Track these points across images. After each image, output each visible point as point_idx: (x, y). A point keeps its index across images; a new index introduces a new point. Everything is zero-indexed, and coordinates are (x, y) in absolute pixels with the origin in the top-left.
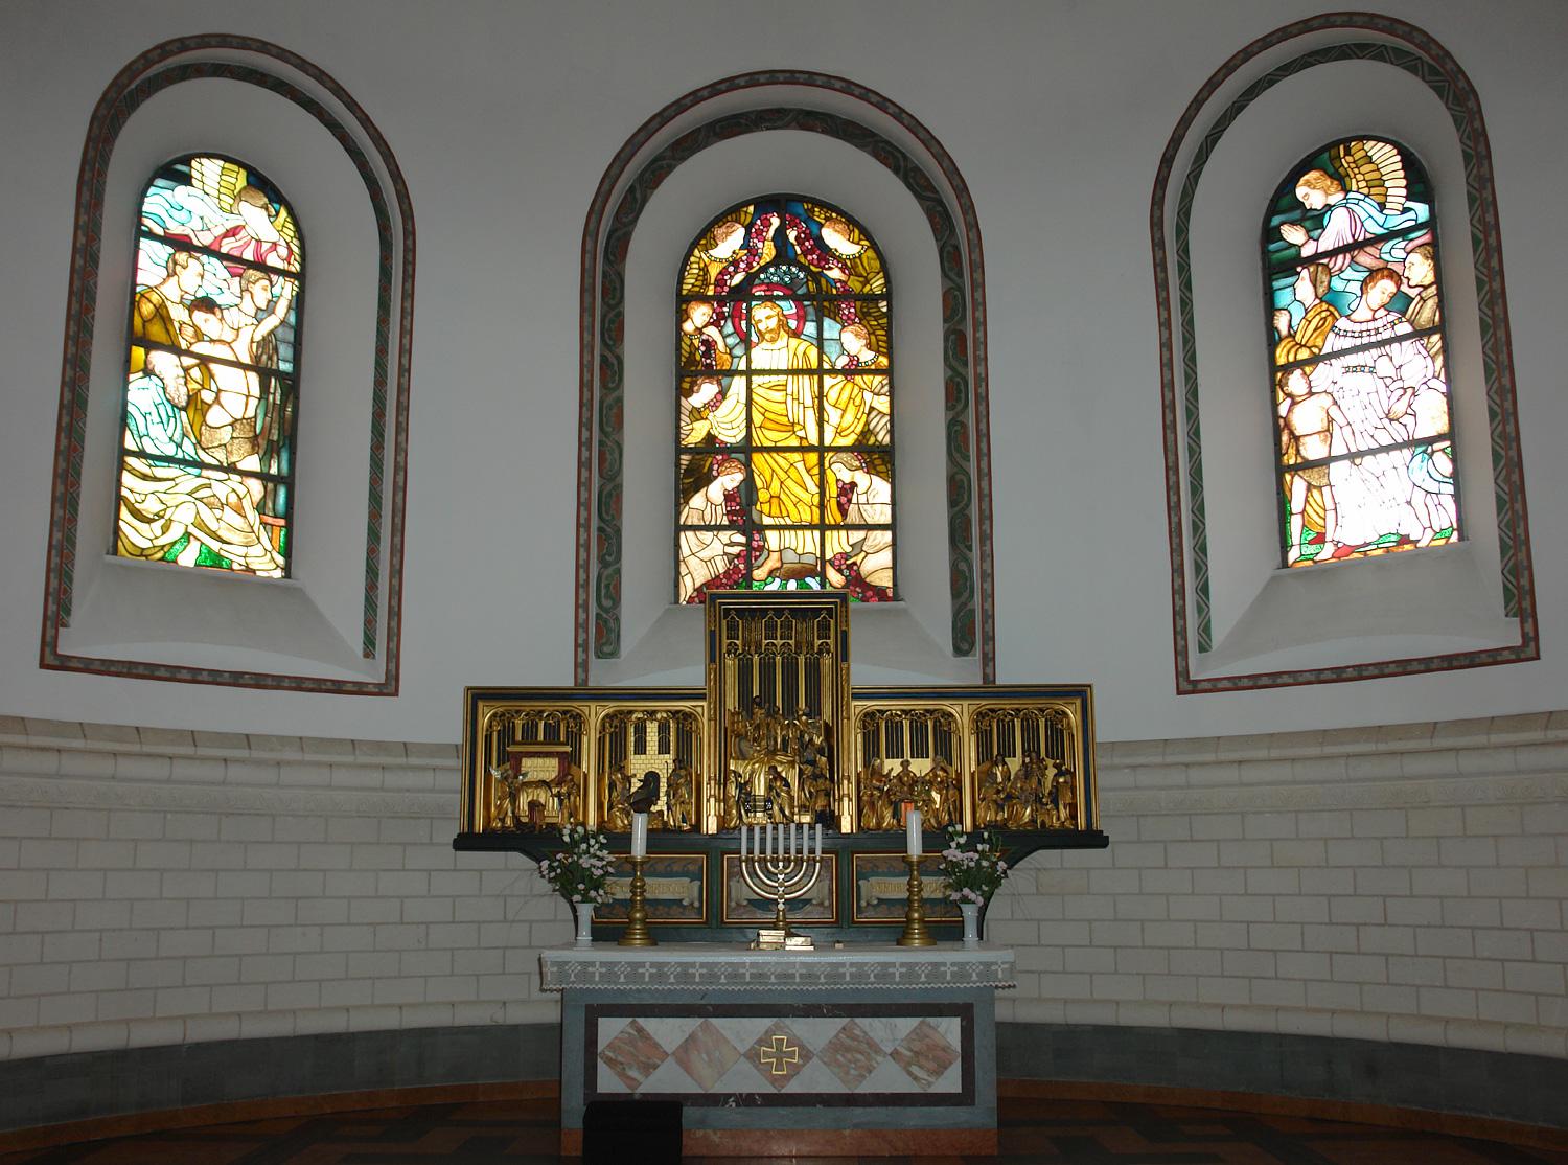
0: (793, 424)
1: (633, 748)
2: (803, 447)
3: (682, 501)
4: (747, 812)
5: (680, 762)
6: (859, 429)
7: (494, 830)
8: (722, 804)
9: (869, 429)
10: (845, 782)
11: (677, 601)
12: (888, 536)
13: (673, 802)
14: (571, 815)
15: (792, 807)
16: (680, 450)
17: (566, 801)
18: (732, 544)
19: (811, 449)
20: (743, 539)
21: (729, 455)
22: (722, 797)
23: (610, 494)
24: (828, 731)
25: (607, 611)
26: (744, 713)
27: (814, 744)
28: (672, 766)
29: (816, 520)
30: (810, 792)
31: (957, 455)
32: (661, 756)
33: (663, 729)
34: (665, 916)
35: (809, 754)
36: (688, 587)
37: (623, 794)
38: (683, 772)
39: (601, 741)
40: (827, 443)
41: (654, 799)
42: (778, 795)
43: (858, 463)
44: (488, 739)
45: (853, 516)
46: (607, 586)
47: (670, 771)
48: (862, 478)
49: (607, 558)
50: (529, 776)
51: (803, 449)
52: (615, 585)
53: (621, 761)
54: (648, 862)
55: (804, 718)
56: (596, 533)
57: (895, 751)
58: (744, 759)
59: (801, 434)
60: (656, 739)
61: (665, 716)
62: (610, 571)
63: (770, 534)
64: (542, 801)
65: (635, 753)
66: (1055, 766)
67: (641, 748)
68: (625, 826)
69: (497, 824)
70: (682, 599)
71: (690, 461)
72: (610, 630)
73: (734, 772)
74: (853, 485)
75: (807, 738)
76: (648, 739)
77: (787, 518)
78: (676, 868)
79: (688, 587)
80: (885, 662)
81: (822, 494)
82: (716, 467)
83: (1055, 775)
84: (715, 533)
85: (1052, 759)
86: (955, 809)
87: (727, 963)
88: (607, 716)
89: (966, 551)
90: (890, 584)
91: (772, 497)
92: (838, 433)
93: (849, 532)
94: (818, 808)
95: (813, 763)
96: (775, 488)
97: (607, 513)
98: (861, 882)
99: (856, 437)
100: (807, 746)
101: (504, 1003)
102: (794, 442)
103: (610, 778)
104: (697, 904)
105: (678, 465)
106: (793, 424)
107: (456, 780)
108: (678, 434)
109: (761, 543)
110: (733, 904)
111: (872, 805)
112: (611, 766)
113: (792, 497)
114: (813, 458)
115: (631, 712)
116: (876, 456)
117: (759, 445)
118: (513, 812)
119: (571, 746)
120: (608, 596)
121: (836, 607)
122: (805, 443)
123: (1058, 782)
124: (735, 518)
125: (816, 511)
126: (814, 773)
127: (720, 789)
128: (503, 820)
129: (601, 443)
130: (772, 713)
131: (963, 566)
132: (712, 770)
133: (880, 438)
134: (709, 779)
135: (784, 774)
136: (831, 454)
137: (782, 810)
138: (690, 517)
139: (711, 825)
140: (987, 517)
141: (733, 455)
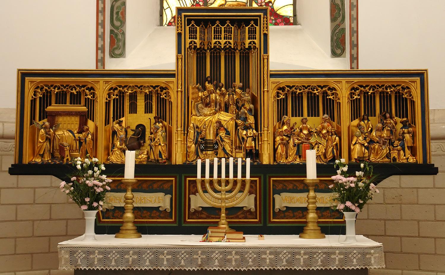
25: (117, 28)
33: (148, 98)
46: (117, 13)
57: (298, 112)
67: (133, 109)
69: (283, 161)
70: (164, 23)
72: (119, 40)
90: (292, 15)
120: (118, 19)
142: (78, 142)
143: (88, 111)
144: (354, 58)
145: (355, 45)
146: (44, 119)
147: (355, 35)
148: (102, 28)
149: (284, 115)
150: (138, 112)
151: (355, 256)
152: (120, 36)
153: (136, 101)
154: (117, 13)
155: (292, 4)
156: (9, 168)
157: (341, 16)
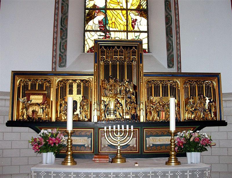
0: (119, 2)
1: (68, 92)
2: (122, 9)
3: (86, 23)
4: (108, 114)
5: (85, 97)
6: (138, 5)
7: (20, 120)
8: (99, 112)
9: (141, 4)
10: (142, 104)
11: (84, 52)
12: (146, 34)
13: (82, 111)
14: (46, 115)
15: (123, 113)
16: (86, 9)
17: (45, 110)
18: (101, 36)
19: (124, 9)
20: (104, 34)
21: (100, 10)
23: (64, 19)
24: (135, 87)
25: (63, 53)
26: (107, 81)
27: (130, 92)
28: (81, 99)
29: (125, 29)
30: (130, 108)
31: (168, 10)
32: (78, 95)
33: (79, 86)
34: (79, 150)
35: (129, 95)
36: (87, 48)
37: (64, 108)
38: (85, 101)
39: (57, 90)
40: (128, 8)
41: (75, 110)
43: (137, 14)
44: (19, 89)
45: (136, 29)
47: (81, 100)
48: (138, 18)
49: (63, 37)
50: (33, 101)
51: (122, 9)
53: (64, 97)
54: (74, 132)
55: (127, 83)
56: (60, 30)
57: (157, 94)
58: (107, 96)
59: (121, 5)
60: (76, 89)
61: (79, 81)
62: (64, 41)
63: (111, 33)
64: (37, 110)
65: (69, 94)
66: (209, 99)
67: (71, 92)
68: (65, 119)
69: (21, 118)
70: (85, 52)
71: (88, 12)
72: (63, 59)
73: (103, 100)
74: (136, 20)
75: (128, 89)
76: (73, 89)
77: (117, 28)
78: (83, 133)
79: (87, 48)
80: (156, 62)
81: (127, 22)
82: (96, 14)
83: (209, 102)
84: (96, 32)
85: (208, 97)
86: (178, 114)
87: (104, 173)
88: (59, 81)
89: (171, 37)
90: (147, 48)
91: (112, 22)
92: (132, 5)
93: (135, 33)
94: (132, 113)
95: (130, 98)
96: (113, 20)
97: (63, 24)
98: (147, 139)
99: (137, 6)
100: (128, 92)
101: (28, 174)
102: (119, 8)
103: (60, 102)
104: (90, 146)
105: (85, 13)
106: (119, 2)
107: (8, 103)
108: (85, 4)
109: (109, 36)
110: (103, 146)
111: (151, 113)
112: (60, 98)
113: (118, 22)
114: (124, 12)
115: (68, 80)
116: (143, 12)
117: (109, 8)
118: (27, 114)
119: (47, 92)
120: (63, 49)
121: (138, 45)
122: (122, 8)
123: (210, 105)
124: (101, 28)
125: (125, 27)
128: (23, 116)
129: (62, 4)
130: (116, 81)
131: (170, 42)
132: (96, 100)
133: (144, 7)
134: (94, 103)
135: (120, 102)
136: (130, 11)
137: (120, 114)
138: (88, 27)
139: (95, 119)
140: (178, 27)
141: (101, 11)
142: (42, 109)
143: (47, 93)
144: (179, 68)
145: (179, 62)
146: (24, 97)
147: (179, 57)
148: (55, 52)
149: (150, 96)
150: (73, 94)
151: (197, 172)
152: (64, 57)
153: (72, 88)
156: (6, 123)
157: (172, 49)
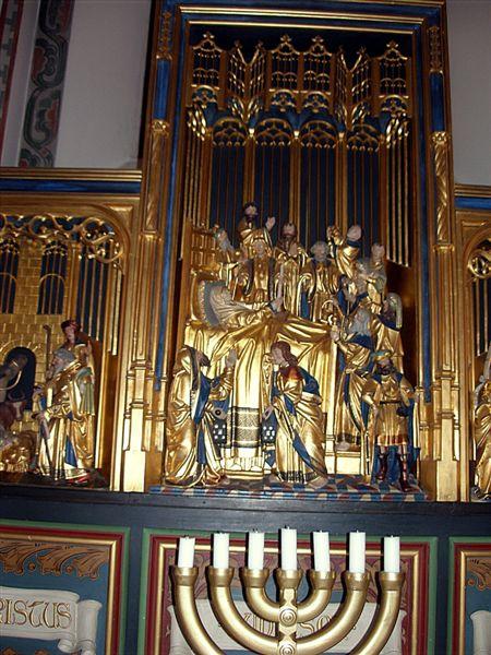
4: (219, 444)
8: (161, 426)
15: (320, 438)
22: (162, 408)
25: (37, 146)
30: (365, 408)
42: (291, 408)
46: (41, 114)
52: (53, 112)
58: (217, 329)
62: (46, 94)
73: (192, 352)
94: (384, 444)
95: (367, 342)
120: (41, 127)
126: (370, 364)
127: (157, 391)
135: (304, 364)
137: (298, 445)
154: (41, 114)
155: (126, 489)
